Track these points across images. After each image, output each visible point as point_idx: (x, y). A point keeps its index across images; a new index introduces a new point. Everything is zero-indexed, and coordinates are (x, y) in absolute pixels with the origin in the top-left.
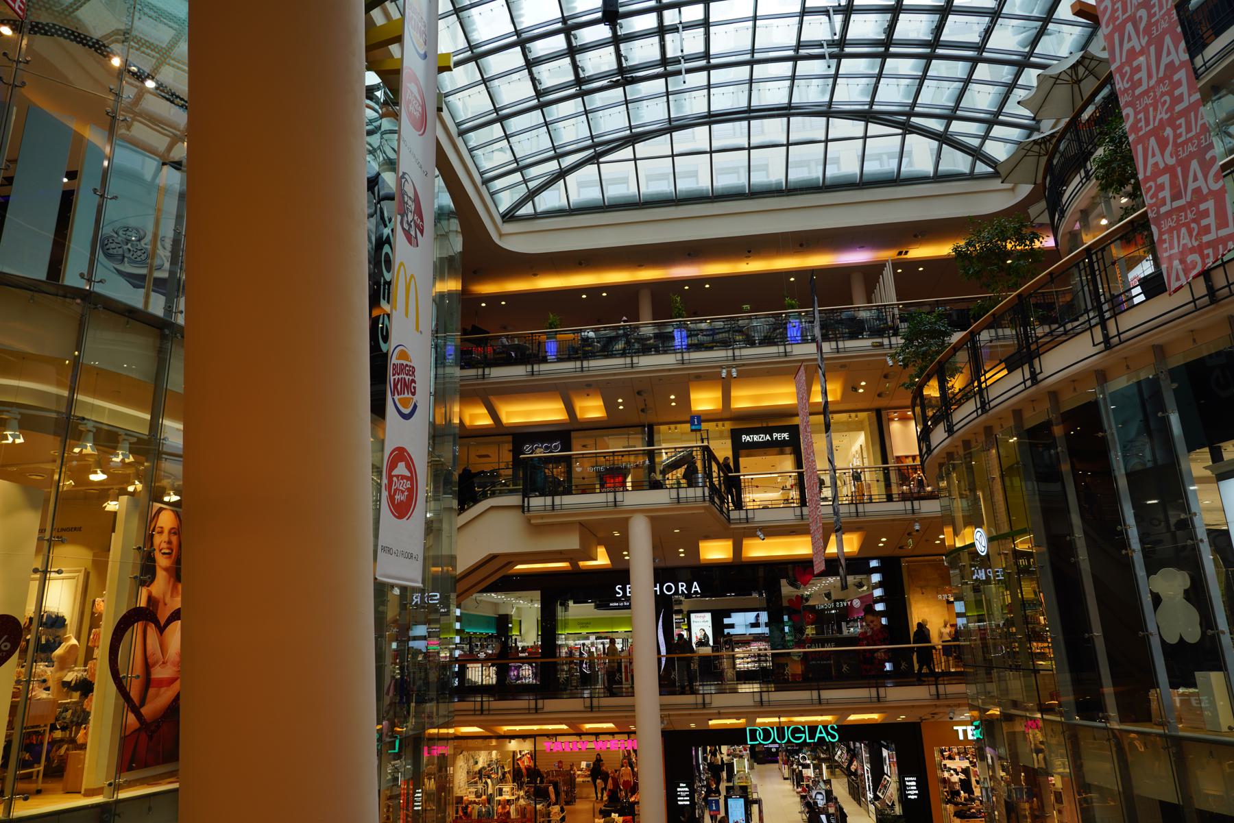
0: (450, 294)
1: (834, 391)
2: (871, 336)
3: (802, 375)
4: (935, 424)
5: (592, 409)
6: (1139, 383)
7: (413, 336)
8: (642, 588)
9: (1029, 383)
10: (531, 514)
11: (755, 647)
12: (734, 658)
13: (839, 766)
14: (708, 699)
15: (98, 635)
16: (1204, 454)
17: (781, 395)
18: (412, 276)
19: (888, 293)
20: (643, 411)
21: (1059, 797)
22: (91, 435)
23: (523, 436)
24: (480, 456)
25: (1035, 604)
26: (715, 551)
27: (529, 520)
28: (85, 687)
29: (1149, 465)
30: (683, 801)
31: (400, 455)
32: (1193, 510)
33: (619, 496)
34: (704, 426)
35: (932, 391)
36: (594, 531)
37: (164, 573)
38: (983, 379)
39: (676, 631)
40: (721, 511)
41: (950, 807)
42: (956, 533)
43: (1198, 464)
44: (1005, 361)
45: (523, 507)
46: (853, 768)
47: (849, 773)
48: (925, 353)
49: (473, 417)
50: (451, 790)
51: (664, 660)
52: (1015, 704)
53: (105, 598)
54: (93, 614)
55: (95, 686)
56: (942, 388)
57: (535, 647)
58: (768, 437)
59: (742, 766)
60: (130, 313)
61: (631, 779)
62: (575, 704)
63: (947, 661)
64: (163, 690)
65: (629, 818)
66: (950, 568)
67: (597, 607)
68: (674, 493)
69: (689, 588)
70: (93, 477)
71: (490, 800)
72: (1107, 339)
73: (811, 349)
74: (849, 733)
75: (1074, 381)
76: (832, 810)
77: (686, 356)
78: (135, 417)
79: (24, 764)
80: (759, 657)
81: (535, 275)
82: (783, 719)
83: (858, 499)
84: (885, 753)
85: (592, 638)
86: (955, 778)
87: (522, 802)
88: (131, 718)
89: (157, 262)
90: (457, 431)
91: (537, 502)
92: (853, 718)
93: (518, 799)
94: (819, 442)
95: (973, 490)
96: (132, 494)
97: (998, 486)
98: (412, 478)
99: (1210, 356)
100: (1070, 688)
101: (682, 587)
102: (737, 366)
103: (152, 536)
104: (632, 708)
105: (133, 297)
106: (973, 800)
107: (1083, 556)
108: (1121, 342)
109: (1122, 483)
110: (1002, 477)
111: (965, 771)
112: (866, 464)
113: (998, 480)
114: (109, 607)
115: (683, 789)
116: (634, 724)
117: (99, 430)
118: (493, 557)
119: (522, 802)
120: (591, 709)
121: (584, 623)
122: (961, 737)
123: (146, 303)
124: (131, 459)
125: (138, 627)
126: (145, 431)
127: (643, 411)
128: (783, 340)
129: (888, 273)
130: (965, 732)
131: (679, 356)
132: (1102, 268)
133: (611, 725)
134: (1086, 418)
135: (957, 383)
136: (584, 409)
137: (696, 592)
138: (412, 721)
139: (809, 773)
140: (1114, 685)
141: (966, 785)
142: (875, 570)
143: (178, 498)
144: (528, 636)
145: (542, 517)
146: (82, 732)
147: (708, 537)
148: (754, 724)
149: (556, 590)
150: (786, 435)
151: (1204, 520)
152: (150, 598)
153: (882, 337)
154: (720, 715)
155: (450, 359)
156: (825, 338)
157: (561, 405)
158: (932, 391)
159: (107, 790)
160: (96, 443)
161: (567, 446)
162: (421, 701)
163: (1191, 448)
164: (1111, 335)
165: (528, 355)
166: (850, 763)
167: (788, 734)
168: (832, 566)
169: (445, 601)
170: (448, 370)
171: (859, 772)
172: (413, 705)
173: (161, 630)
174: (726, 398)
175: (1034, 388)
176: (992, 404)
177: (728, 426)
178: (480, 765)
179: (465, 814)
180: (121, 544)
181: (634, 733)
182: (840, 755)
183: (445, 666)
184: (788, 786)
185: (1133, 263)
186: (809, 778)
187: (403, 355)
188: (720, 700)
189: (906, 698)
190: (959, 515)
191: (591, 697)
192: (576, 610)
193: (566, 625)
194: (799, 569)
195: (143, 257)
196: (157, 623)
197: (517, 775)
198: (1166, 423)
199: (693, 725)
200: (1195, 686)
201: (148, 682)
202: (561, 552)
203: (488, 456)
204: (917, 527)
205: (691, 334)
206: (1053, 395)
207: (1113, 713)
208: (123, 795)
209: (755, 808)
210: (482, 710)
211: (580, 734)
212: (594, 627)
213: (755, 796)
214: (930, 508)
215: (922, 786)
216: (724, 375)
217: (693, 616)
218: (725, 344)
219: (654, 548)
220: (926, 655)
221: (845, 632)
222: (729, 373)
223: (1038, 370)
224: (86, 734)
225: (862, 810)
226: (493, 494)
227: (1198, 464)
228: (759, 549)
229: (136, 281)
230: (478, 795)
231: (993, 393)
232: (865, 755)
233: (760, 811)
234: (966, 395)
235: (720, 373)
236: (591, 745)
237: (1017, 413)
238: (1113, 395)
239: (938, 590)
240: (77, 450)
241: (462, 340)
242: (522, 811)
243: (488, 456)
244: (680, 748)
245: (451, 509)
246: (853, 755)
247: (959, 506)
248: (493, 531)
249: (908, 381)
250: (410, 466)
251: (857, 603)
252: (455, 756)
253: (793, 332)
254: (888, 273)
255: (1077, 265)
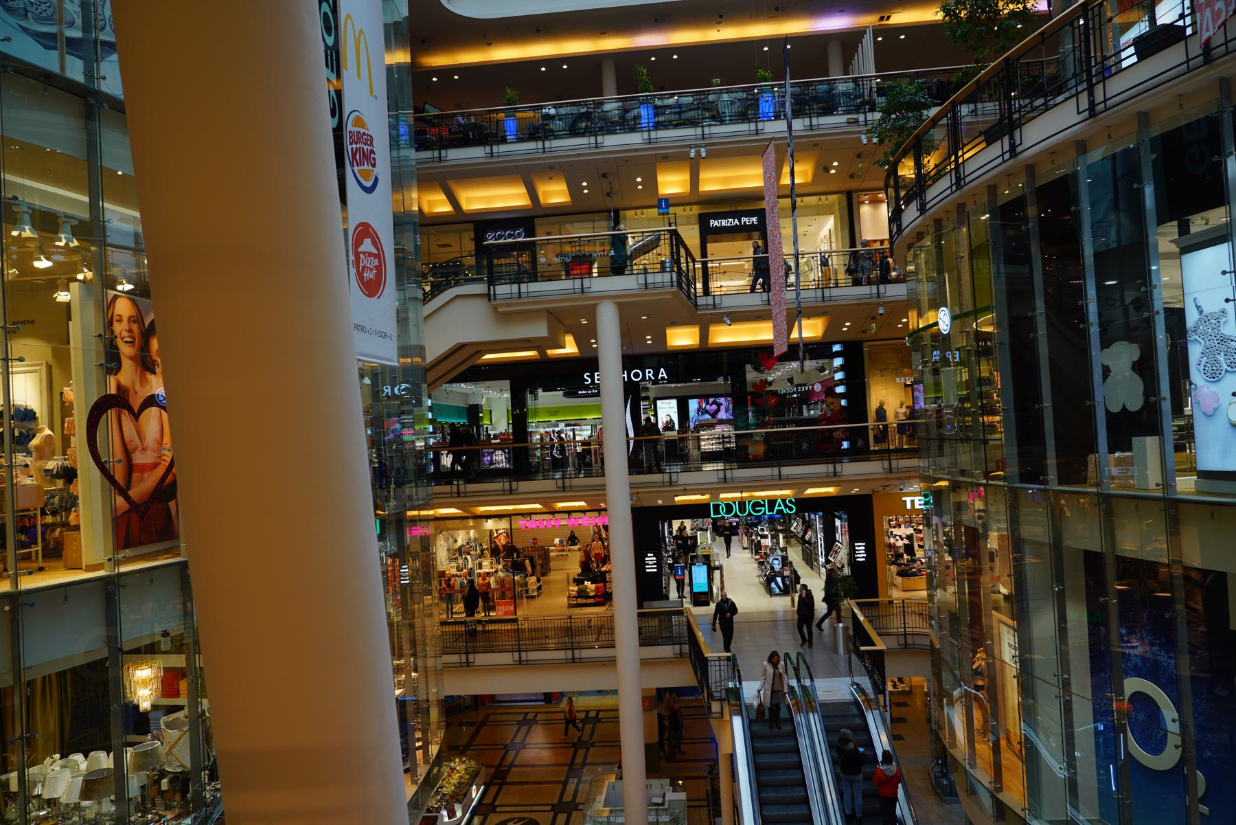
0: (400, 67)
1: (805, 172)
2: (847, 112)
3: (771, 153)
4: (907, 204)
5: (555, 193)
6: (1114, 156)
7: (369, 106)
8: (611, 375)
9: (1007, 156)
10: (497, 302)
11: (719, 430)
12: (698, 439)
13: (795, 536)
14: (674, 477)
15: (72, 424)
16: (1172, 228)
17: (747, 177)
18: (361, 32)
19: (866, 63)
20: (608, 195)
21: (992, 555)
22: (27, 217)
23: (484, 223)
24: (441, 246)
25: (989, 382)
26: (682, 338)
27: (495, 308)
28: (69, 474)
29: (1113, 246)
30: (651, 569)
31: (365, 231)
32: (1154, 282)
33: (586, 282)
34: (672, 210)
35: (907, 170)
36: (562, 319)
37: (130, 362)
38: (960, 153)
39: (643, 417)
40: (689, 297)
41: (894, 568)
42: (920, 315)
43: (1164, 239)
44: (985, 133)
45: (489, 295)
46: (807, 537)
47: (803, 541)
48: (902, 128)
49: (430, 203)
50: (434, 567)
51: (632, 442)
52: (963, 473)
53: (73, 387)
54: (63, 403)
55: (79, 472)
56: (919, 165)
57: (506, 434)
58: (736, 222)
59: (705, 539)
60: (46, 78)
61: (602, 552)
62: (549, 485)
63: (901, 439)
64: (146, 474)
65: (601, 585)
66: (911, 350)
67: (566, 395)
68: (641, 279)
69: (656, 374)
70: (37, 264)
71: (470, 572)
72: (1092, 105)
73: (781, 126)
74: (805, 505)
75: (1052, 153)
76: (787, 573)
77: (653, 135)
78: (70, 199)
79: (22, 545)
80: (723, 439)
81: (489, 44)
82: (745, 494)
83: (826, 282)
84: (838, 522)
85: (562, 426)
86: (900, 543)
87: (501, 574)
88: (120, 500)
89: (67, 18)
90: (417, 220)
91: (502, 290)
92: (811, 491)
93: (497, 572)
94: (786, 229)
95: (940, 271)
96: (84, 282)
97: (965, 268)
98: (379, 256)
99: (1189, 127)
100: (1016, 460)
101: (649, 373)
102: (706, 145)
103: (111, 324)
104: (603, 487)
105: (48, 60)
106: (915, 561)
107: (1042, 330)
108: (1106, 109)
109: (1089, 259)
110: (972, 255)
111: (909, 537)
112: (834, 248)
113: (966, 258)
114: (80, 397)
115: (651, 558)
116: (605, 501)
117: (34, 210)
118: (461, 347)
119: (501, 574)
120: (564, 488)
121: (554, 412)
122: (909, 507)
123: (63, 68)
124: (75, 243)
125: (111, 414)
126: (85, 215)
127: (608, 195)
128: (756, 119)
129: (868, 42)
130: (913, 502)
131: (646, 135)
132: (1097, 26)
133: (583, 503)
134: (1059, 195)
135: (931, 162)
136: (546, 193)
137: (663, 378)
138: (393, 503)
139: (767, 542)
140: (1057, 457)
141: (909, 549)
142: (837, 354)
143: (131, 287)
144: (499, 423)
145: (509, 305)
146: (73, 515)
147: (675, 323)
148: (717, 498)
149: (525, 379)
150: (754, 220)
151: (1162, 297)
152: (119, 386)
153: (858, 113)
154: (685, 492)
155: (404, 140)
156: (797, 114)
157: (522, 190)
158: (907, 170)
159: (109, 565)
160: (34, 227)
161: (531, 232)
162: (399, 485)
163: (1161, 221)
164: (1097, 101)
165: (487, 135)
166: (805, 533)
167: (749, 508)
168: (795, 351)
169: (415, 393)
170: (403, 153)
171: (813, 540)
172: (393, 486)
173: (136, 416)
174: (695, 181)
175: (1012, 161)
176: (967, 180)
177: (696, 210)
178: (459, 543)
179: (449, 585)
180: (81, 332)
181: (605, 510)
182: (796, 526)
183: (420, 454)
184: (747, 554)
185: (1126, 28)
186: (766, 547)
187: (359, 122)
188: (685, 478)
189: (859, 473)
190: (925, 299)
191: (563, 478)
192: (546, 399)
193: (536, 413)
194: (760, 354)
195: (49, 12)
196: (130, 409)
197: (495, 552)
198: (1140, 194)
199: (660, 502)
200: (1130, 450)
201: (130, 468)
202: (529, 340)
203: (449, 245)
204: (881, 311)
205: (658, 110)
206: (1030, 168)
207: (1052, 476)
208: (123, 569)
209: (717, 574)
210: (459, 493)
211: (553, 513)
212: (563, 415)
213: (717, 563)
214: (895, 291)
215: (870, 550)
216: (692, 155)
217: (659, 402)
218: (692, 123)
219: (622, 335)
220: (882, 435)
221: (805, 414)
222: (698, 153)
223: (1018, 142)
224: (78, 516)
225: (813, 573)
226: (457, 284)
227: (1164, 239)
228: (726, 335)
229: (47, 40)
230: (459, 569)
231: (969, 168)
232: (819, 526)
233: (722, 576)
234: (939, 174)
235: (689, 153)
236: (564, 522)
237: (992, 189)
238: (1089, 167)
239: (898, 373)
240: (15, 233)
241: (416, 119)
242: (501, 582)
243: (449, 245)
244: (648, 524)
245: (416, 298)
246: (808, 525)
247: (925, 288)
248: (460, 320)
249: (883, 158)
250: (376, 243)
251: (818, 388)
252: (435, 536)
253: (766, 107)
254: (868, 42)
255: (1071, 24)
